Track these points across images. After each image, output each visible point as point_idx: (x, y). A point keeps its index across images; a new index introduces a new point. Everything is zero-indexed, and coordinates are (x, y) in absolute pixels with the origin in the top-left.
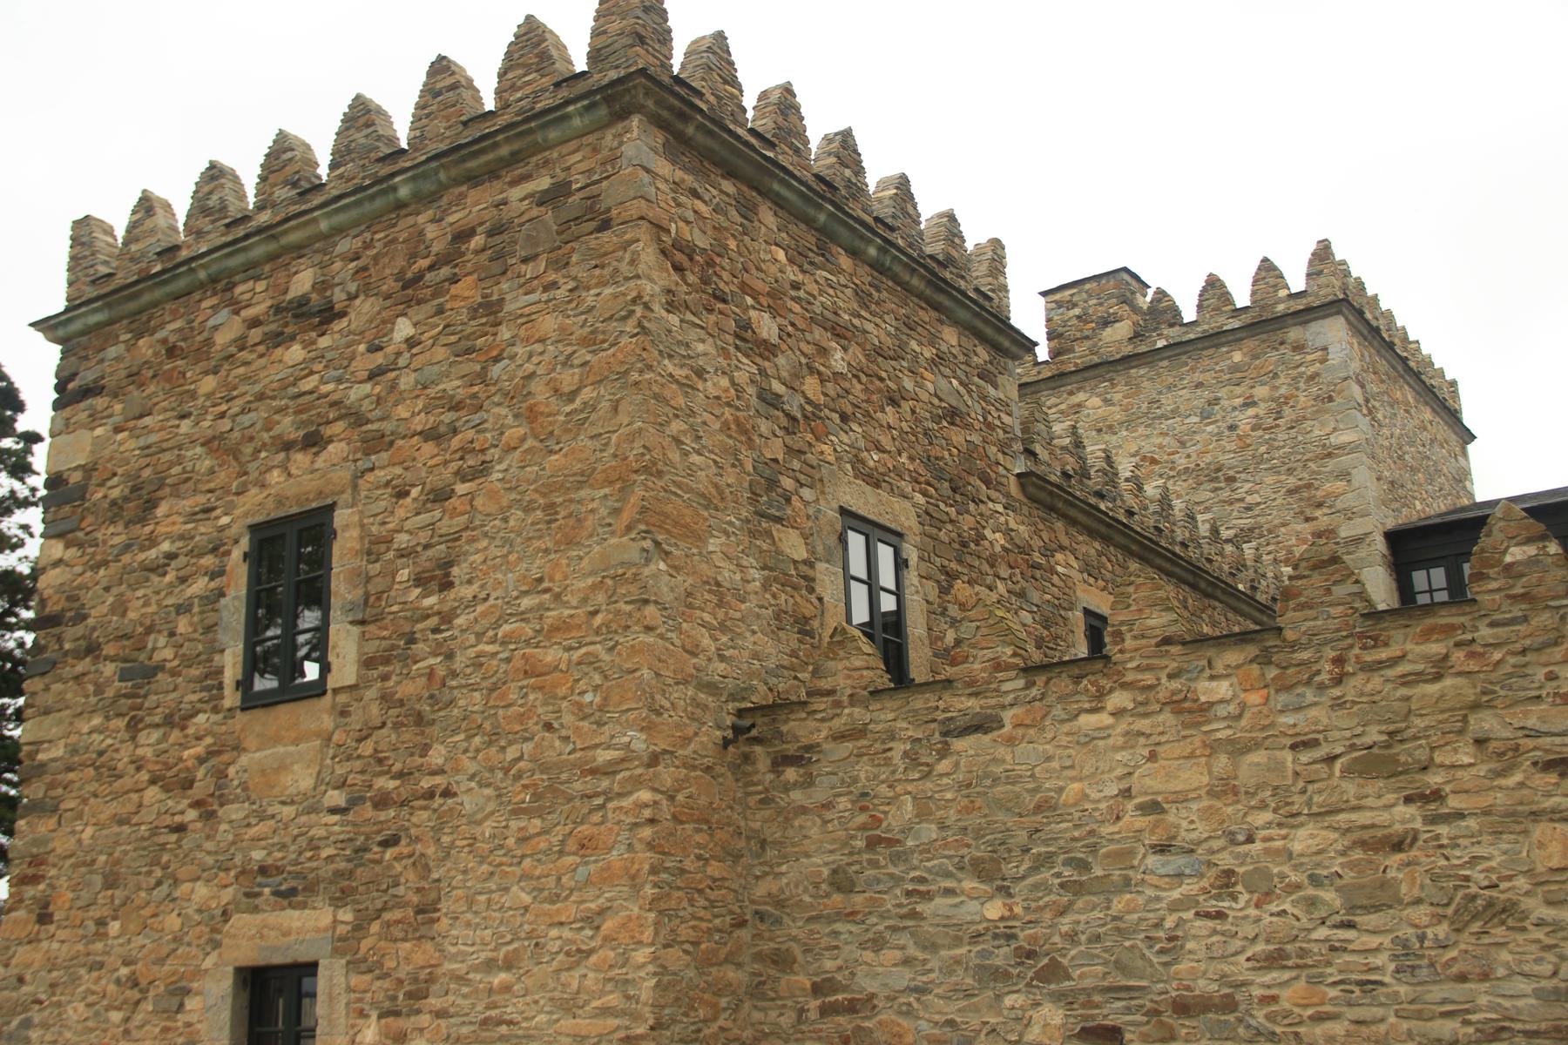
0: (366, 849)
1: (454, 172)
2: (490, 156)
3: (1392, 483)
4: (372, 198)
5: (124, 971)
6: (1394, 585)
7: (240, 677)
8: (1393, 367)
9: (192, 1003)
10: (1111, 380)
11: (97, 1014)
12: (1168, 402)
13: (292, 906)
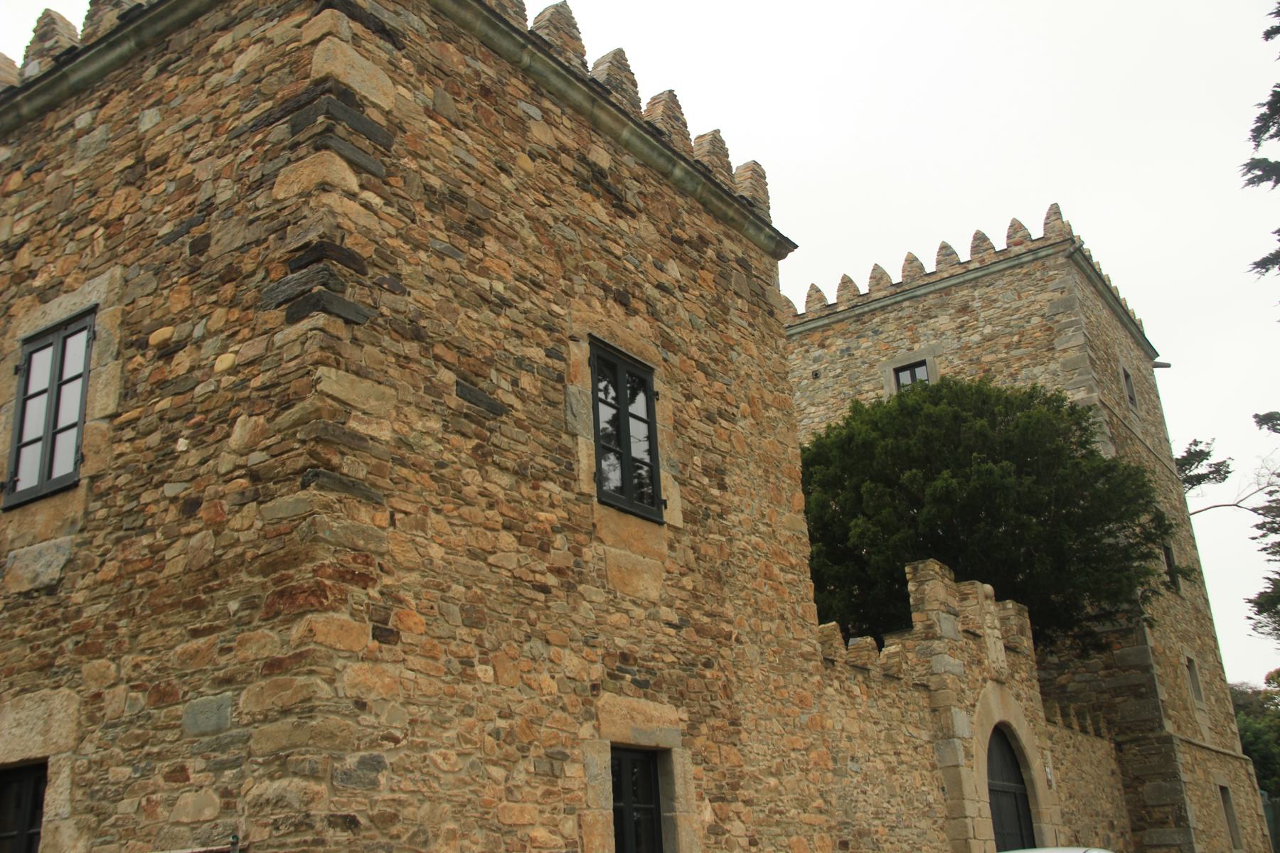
0: (694, 665)
1: (705, 194)
2: (724, 207)
4: (662, 154)
5: (502, 723)
7: (953, 576)
9: (572, 770)
11: (472, 765)
13: (646, 696)
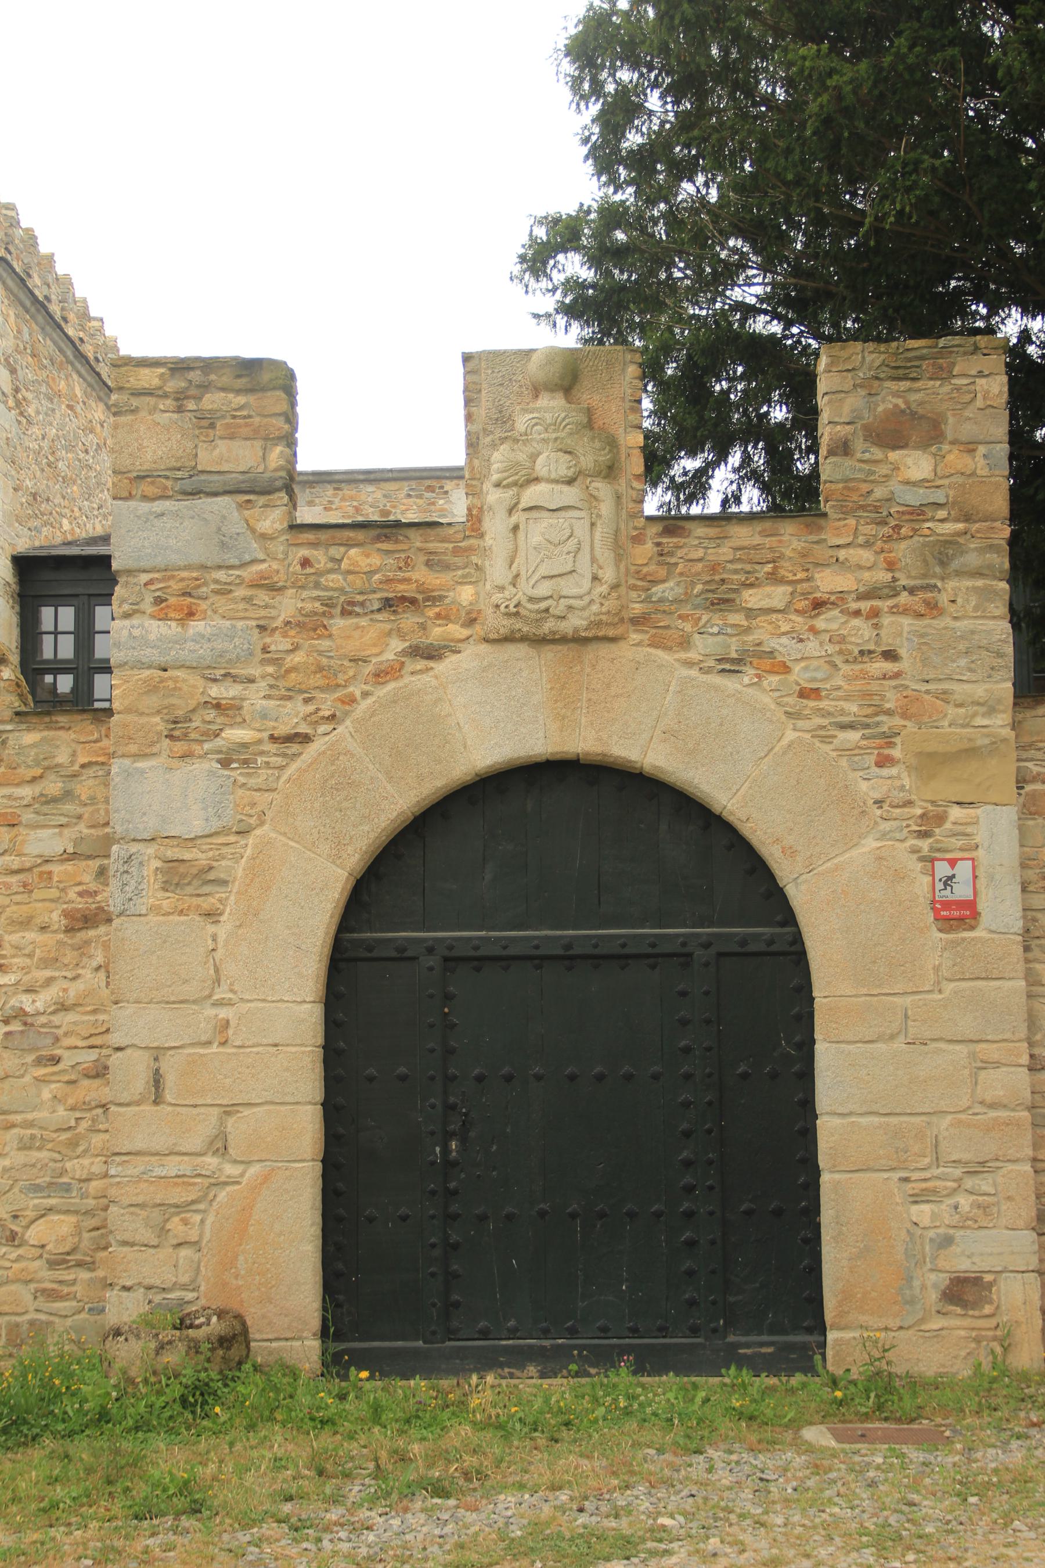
3: (34, 495)
6: (15, 620)
8: (61, 350)
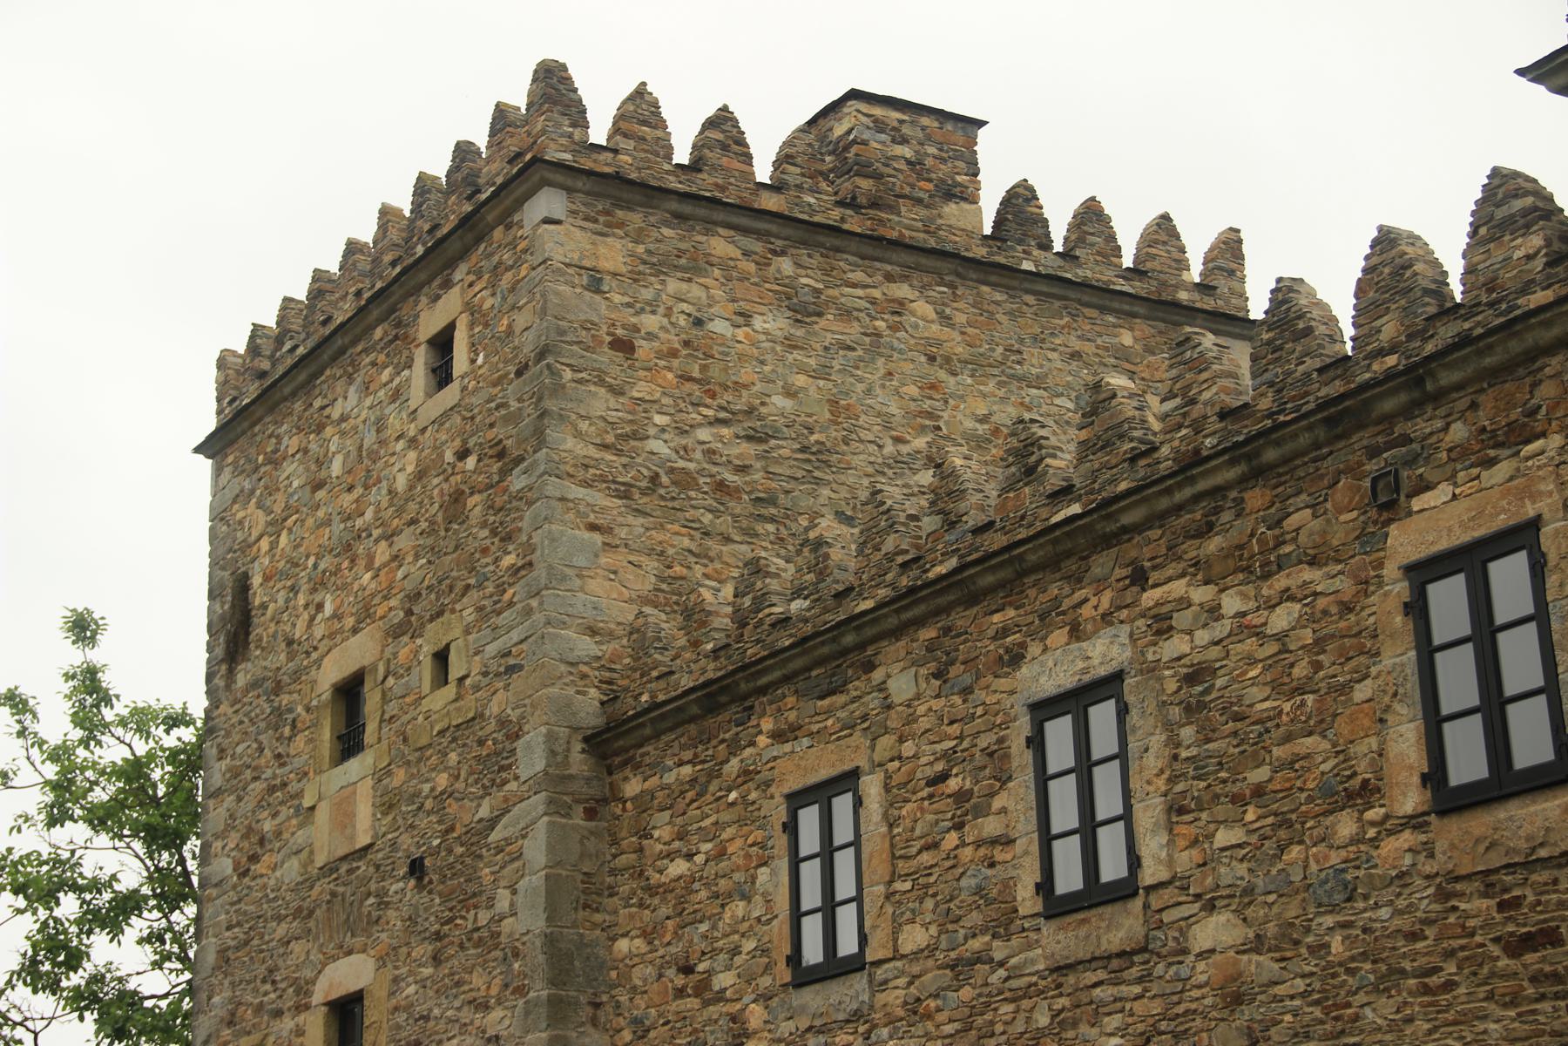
10: (952, 286)
12: (1032, 355)
